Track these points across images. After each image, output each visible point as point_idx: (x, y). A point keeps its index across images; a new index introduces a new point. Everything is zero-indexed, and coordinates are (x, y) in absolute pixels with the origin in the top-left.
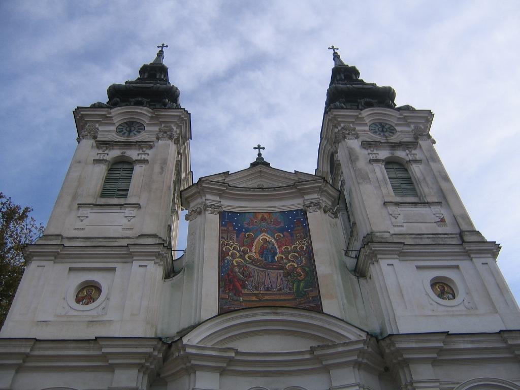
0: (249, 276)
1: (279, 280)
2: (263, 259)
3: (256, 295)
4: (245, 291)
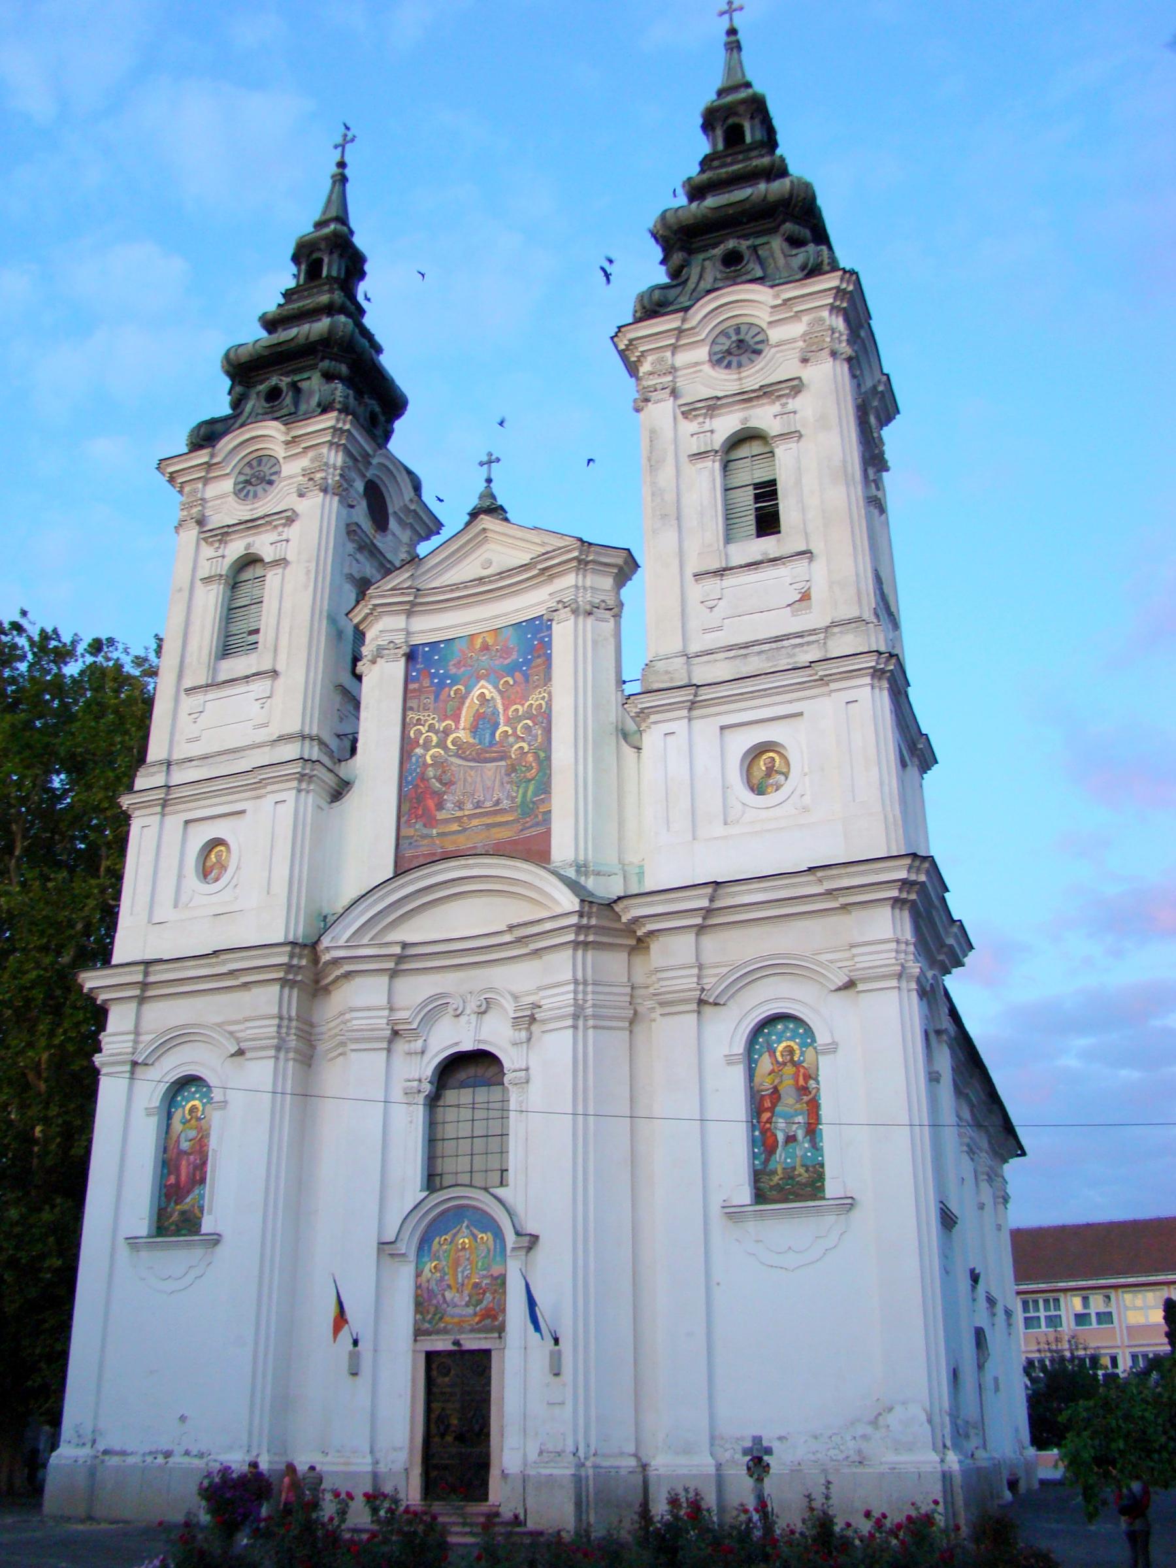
0: (448, 784)
2: (477, 741)
3: (459, 819)
4: (441, 815)
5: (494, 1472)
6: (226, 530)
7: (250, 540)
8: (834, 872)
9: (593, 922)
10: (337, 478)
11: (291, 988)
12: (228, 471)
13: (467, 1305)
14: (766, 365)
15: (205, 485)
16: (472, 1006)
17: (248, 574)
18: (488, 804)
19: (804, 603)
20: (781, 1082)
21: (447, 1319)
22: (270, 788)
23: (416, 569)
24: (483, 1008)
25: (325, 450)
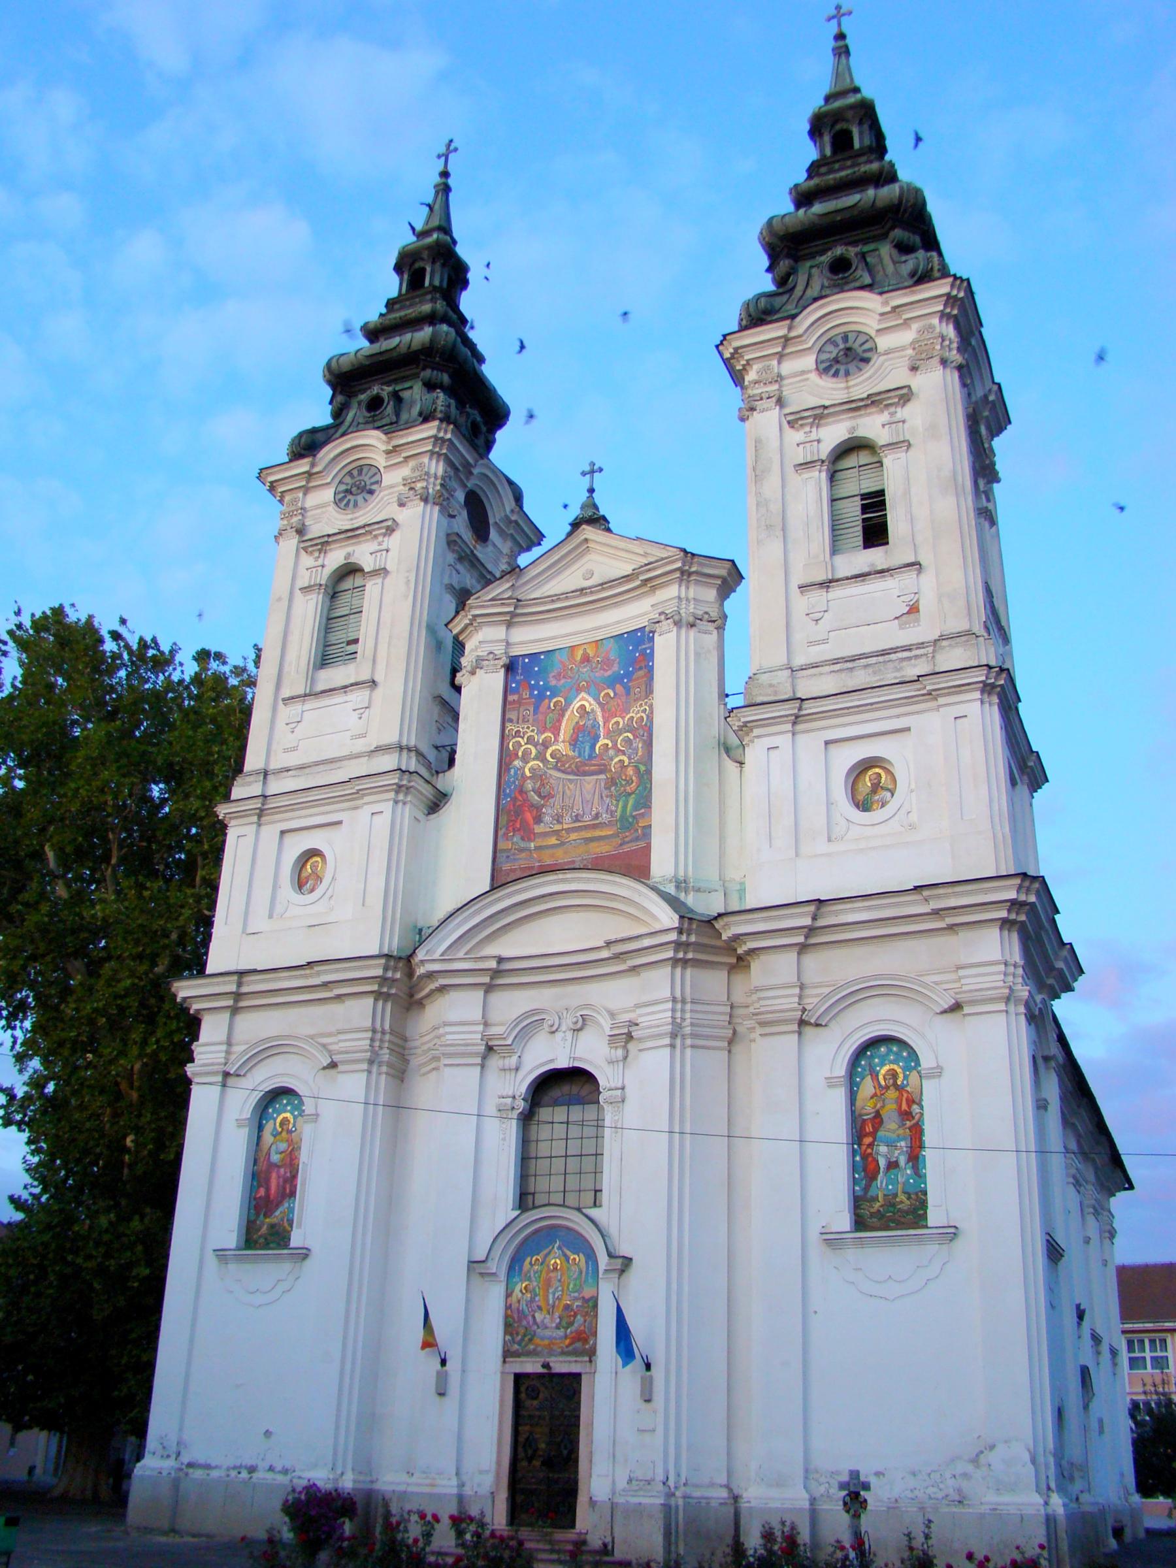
0: (550, 796)
1: (596, 797)
2: (576, 754)
4: (538, 829)
5: (582, 1499)
7: (350, 549)
8: (941, 891)
10: (438, 488)
11: (385, 1001)
13: (558, 1327)
14: (876, 372)
16: (568, 1022)
17: (348, 584)
19: (912, 616)
21: (537, 1340)
25: (426, 460)
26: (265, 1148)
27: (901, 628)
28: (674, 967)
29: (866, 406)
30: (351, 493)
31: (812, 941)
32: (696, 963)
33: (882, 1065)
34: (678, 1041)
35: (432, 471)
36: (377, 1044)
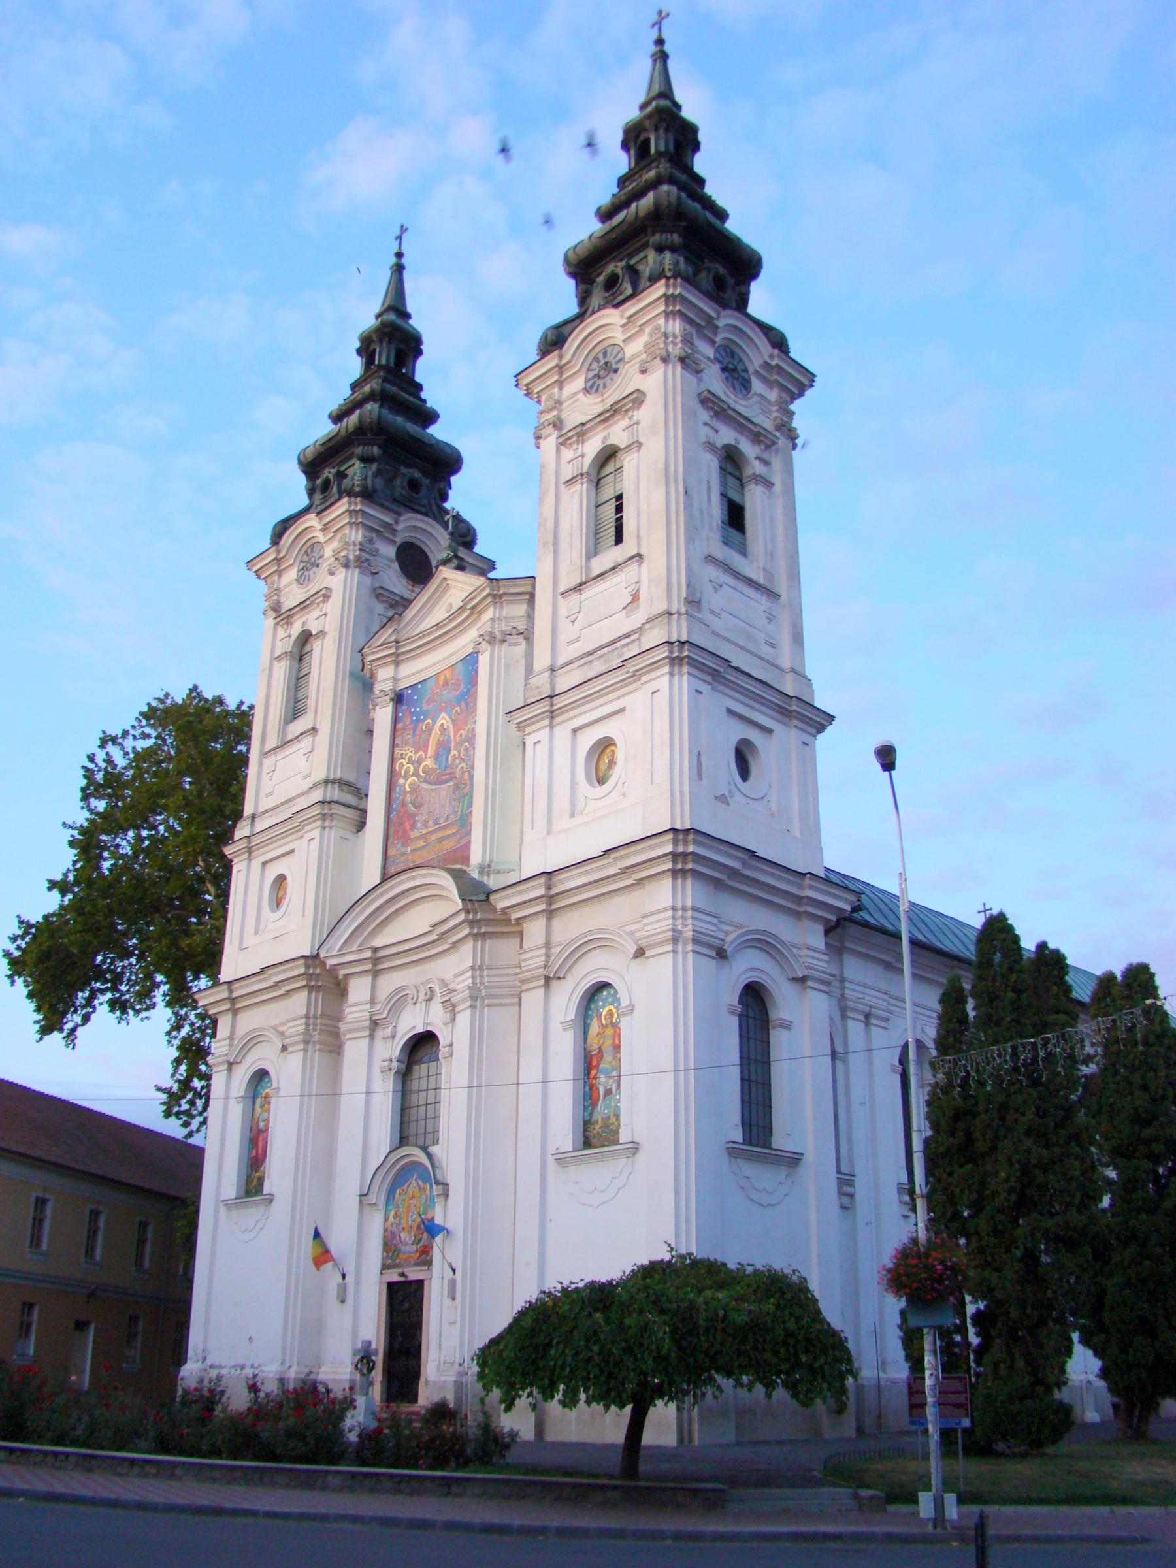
0: (421, 805)
4: (413, 834)
5: (422, 1380)
6: (288, 613)
7: (304, 619)
8: (622, 852)
9: (479, 916)
10: (358, 553)
11: (684, 878)
12: (291, 562)
13: (413, 1244)
14: (622, 381)
15: (280, 576)
16: (422, 997)
17: (610, 468)
18: (442, 820)
19: (635, 604)
20: (604, 1043)
21: (401, 1256)
22: (307, 828)
23: (399, 622)
24: (428, 997)
25: (347, 531)
26: (256, 1116)
27: (627, 617)
28: (674, 878)
29: (612, 416)
30: (600, 377)
31: (555, 906)
32: (493, 935)
33: (604, 1007)
34: (680, 948)
35: (353, 539)
36: (311, 1027)
